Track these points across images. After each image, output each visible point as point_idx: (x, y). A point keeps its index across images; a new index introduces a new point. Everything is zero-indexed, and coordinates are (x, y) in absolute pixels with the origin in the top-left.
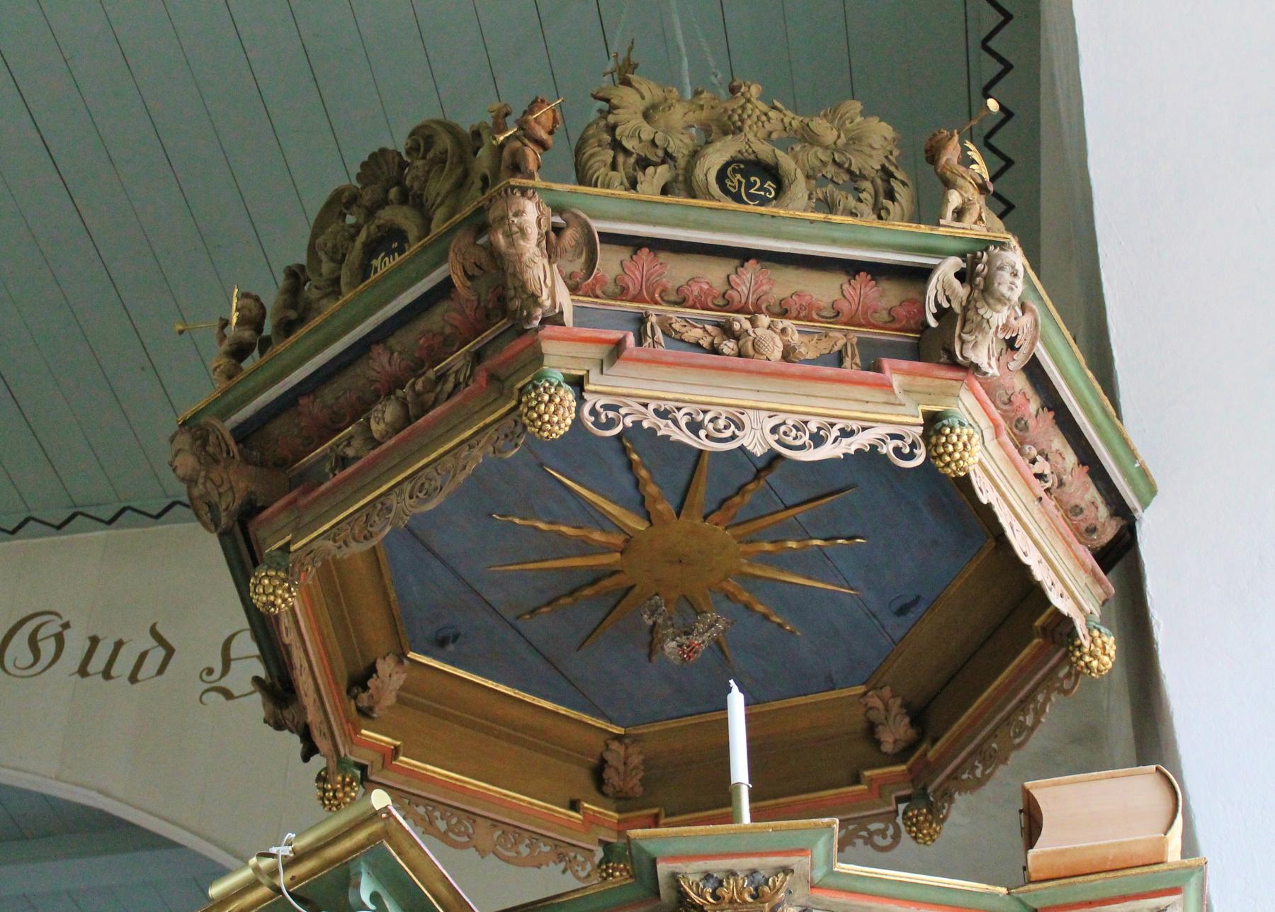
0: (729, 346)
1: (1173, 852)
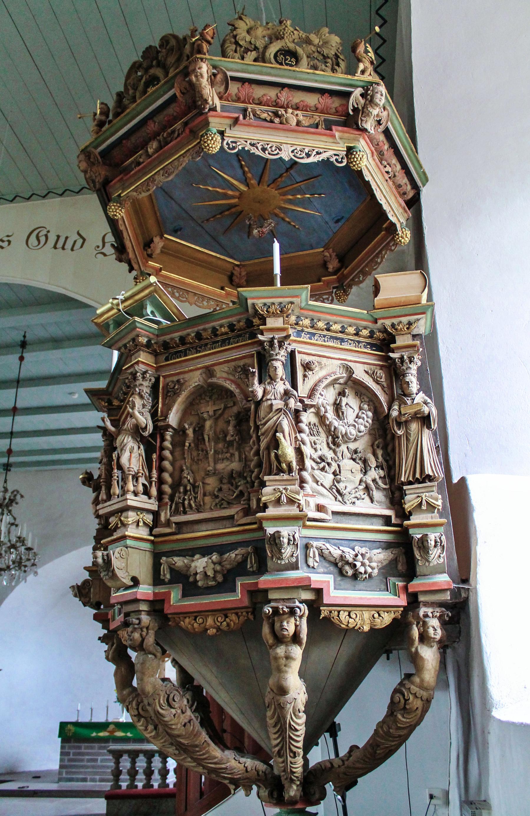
0: (277, 120)
1: (424, 301)
